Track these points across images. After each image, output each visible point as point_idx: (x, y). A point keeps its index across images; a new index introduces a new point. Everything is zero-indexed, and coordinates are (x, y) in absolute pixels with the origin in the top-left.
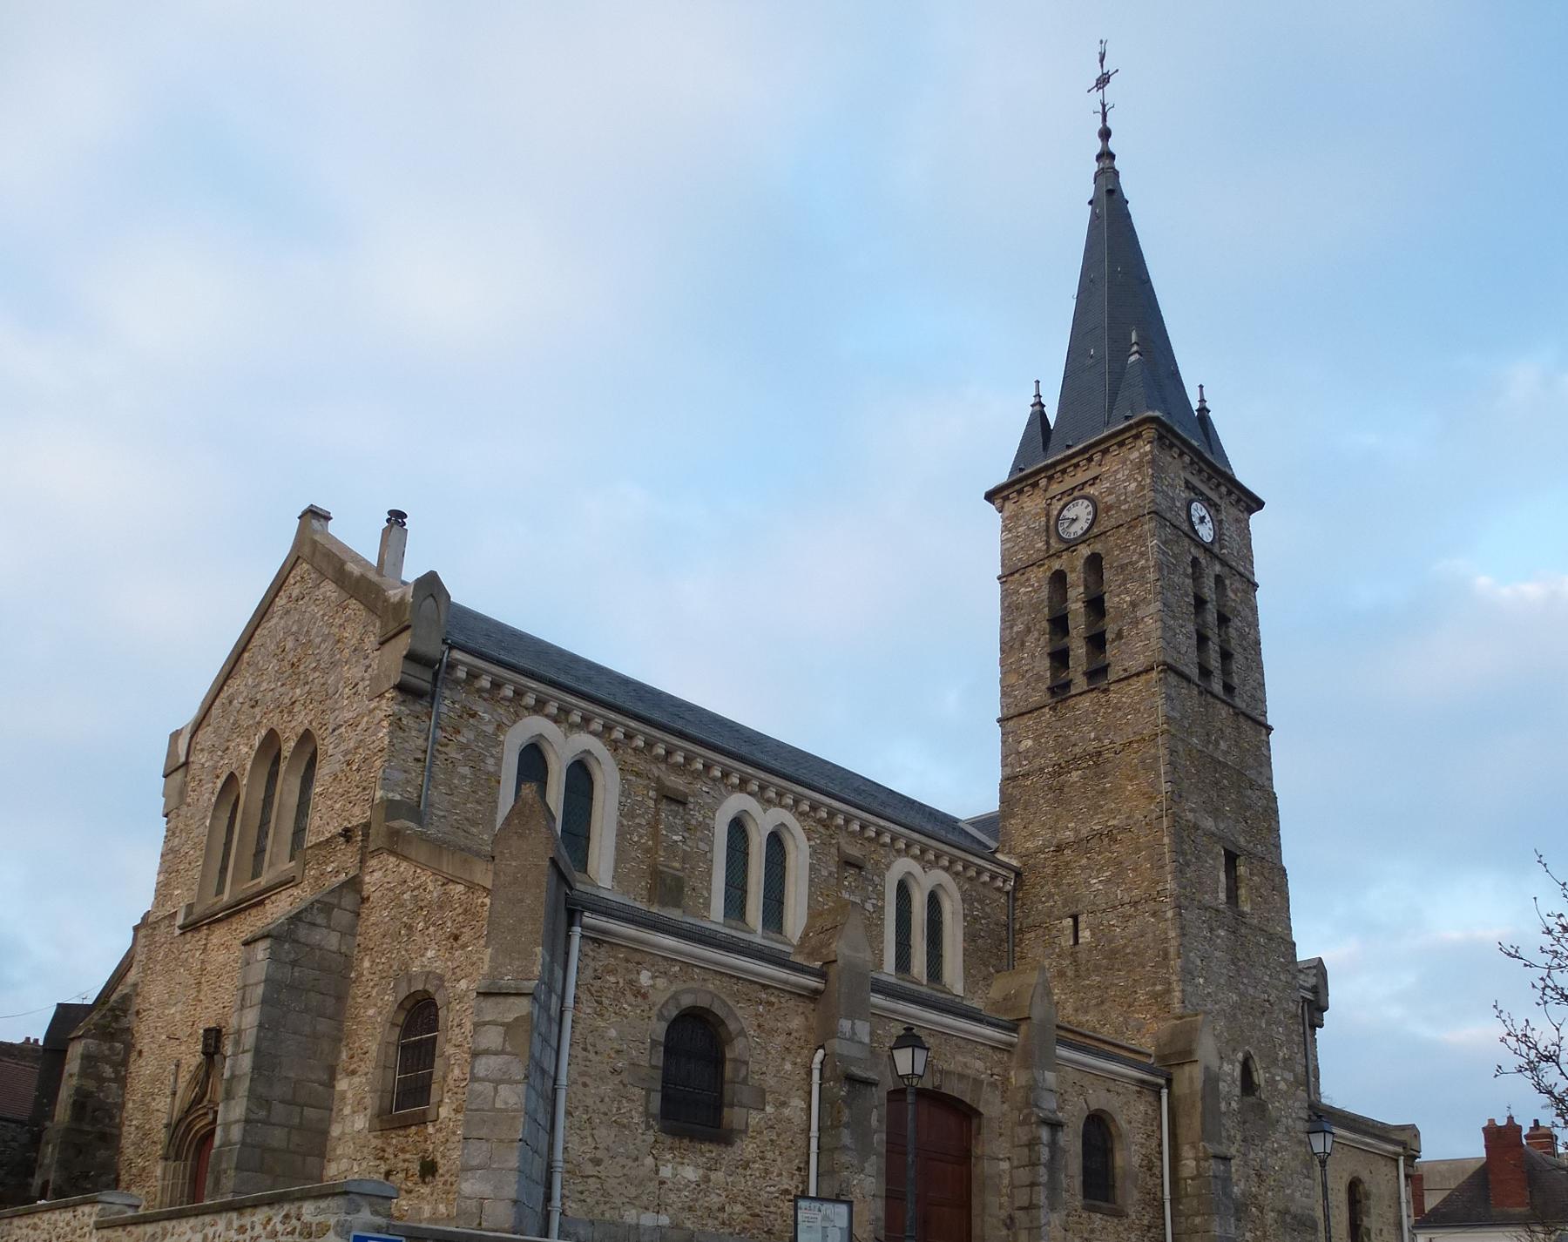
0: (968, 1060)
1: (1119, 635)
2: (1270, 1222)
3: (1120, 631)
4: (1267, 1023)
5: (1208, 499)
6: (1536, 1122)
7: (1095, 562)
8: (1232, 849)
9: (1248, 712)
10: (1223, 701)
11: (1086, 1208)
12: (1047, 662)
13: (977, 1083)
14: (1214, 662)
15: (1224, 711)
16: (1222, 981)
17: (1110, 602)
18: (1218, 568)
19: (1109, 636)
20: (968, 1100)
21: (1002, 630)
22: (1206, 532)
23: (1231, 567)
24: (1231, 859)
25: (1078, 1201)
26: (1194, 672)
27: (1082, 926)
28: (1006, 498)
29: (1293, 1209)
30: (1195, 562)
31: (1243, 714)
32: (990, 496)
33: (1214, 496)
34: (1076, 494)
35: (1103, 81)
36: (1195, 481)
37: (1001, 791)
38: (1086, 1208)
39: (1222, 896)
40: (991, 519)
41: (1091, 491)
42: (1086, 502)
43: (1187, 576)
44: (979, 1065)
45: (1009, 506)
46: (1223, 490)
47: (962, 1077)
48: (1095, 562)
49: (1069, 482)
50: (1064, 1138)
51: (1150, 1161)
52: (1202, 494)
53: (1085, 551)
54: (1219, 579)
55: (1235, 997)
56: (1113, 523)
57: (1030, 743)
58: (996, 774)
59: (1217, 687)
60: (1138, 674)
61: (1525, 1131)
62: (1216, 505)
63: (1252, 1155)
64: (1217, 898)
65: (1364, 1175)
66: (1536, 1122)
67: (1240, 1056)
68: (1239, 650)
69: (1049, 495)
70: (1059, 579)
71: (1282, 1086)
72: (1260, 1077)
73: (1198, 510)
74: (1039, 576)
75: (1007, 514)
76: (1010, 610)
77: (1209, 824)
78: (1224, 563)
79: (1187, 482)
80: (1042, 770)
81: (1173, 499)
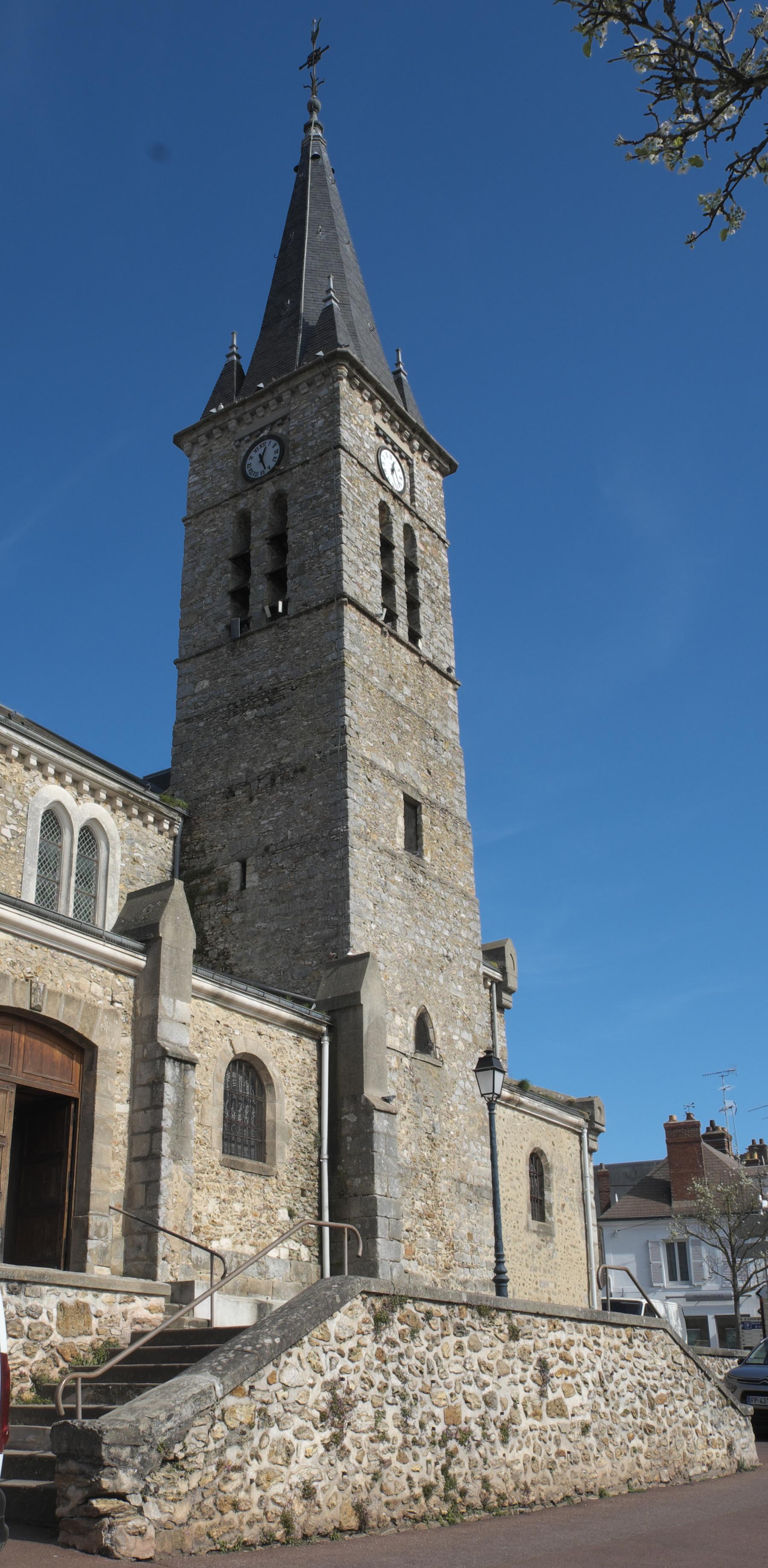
0: (84, 982)
1: (301, 570)
2: (444, 1190)
3: (302, 565)
4: (446, 980)
5: (400, 451)
6: (712, 1123)
7: (280, 502)
8: (414, 796)
9: (435, 662)
10: (408, 647)
11: (223, 1164)
12: (228, 602)
13: (91, 1010)
14: (401, 608)
15: (409, 658)
16: (396, 929)
17: (292, 537)
18: (407, 518)
19: (290, 571)
20: (77, 1028)
21: (185, 572)
22: (397, 481)
23: (421, 520)
24: (412, 808)
25: (216, 1154)
26: (380, 612)
27: (250, 869)
28: (194, 443)
29: (469, 1178)
30: (383, 507)
31: (430, 664)
32: (178, 440)
33: (405, 447)
34: (266, 432)
35: (314, 58)
36: (386, 428)
37: (175, 734)
38: (223, 1164)
39: (400, 841)
40: (179, 463)
41: (280, 431)
42: (273, 442)
43: (373, 517)
44: (97, 989)
45: (198, 452)
46: (416, 444)
47: (70, 1000)
48: (280, 502)
49: (257, 424)
50: (195, 1078)
51: (307, 1117)
52: (393, 443)
53: (270, 488)
54: (408, 530)
55: (410, 948)
56: (300, 459)
57: (206, 683)
58: (170, 716)
59: (402, 631)
60: (318, 608)
61: (703, 1131)
62: (407, 458)
63: (424, 1117)
64: (394, 843)
65: (546, 1147)
66: (712, 1123)
67: (414, 1011)
68: (427, 601)
69: (238, 437)
70: (244, 521)
71: (460, 1046)
72: (438, 1033)
73: (388, 459)
74: (225, 521)
75: (195, 458)
76: (193, 550)
77: (389, 766)
78: (414, 514)
79: (377, 428)
80: (216, 710)
81: (361, 439)
